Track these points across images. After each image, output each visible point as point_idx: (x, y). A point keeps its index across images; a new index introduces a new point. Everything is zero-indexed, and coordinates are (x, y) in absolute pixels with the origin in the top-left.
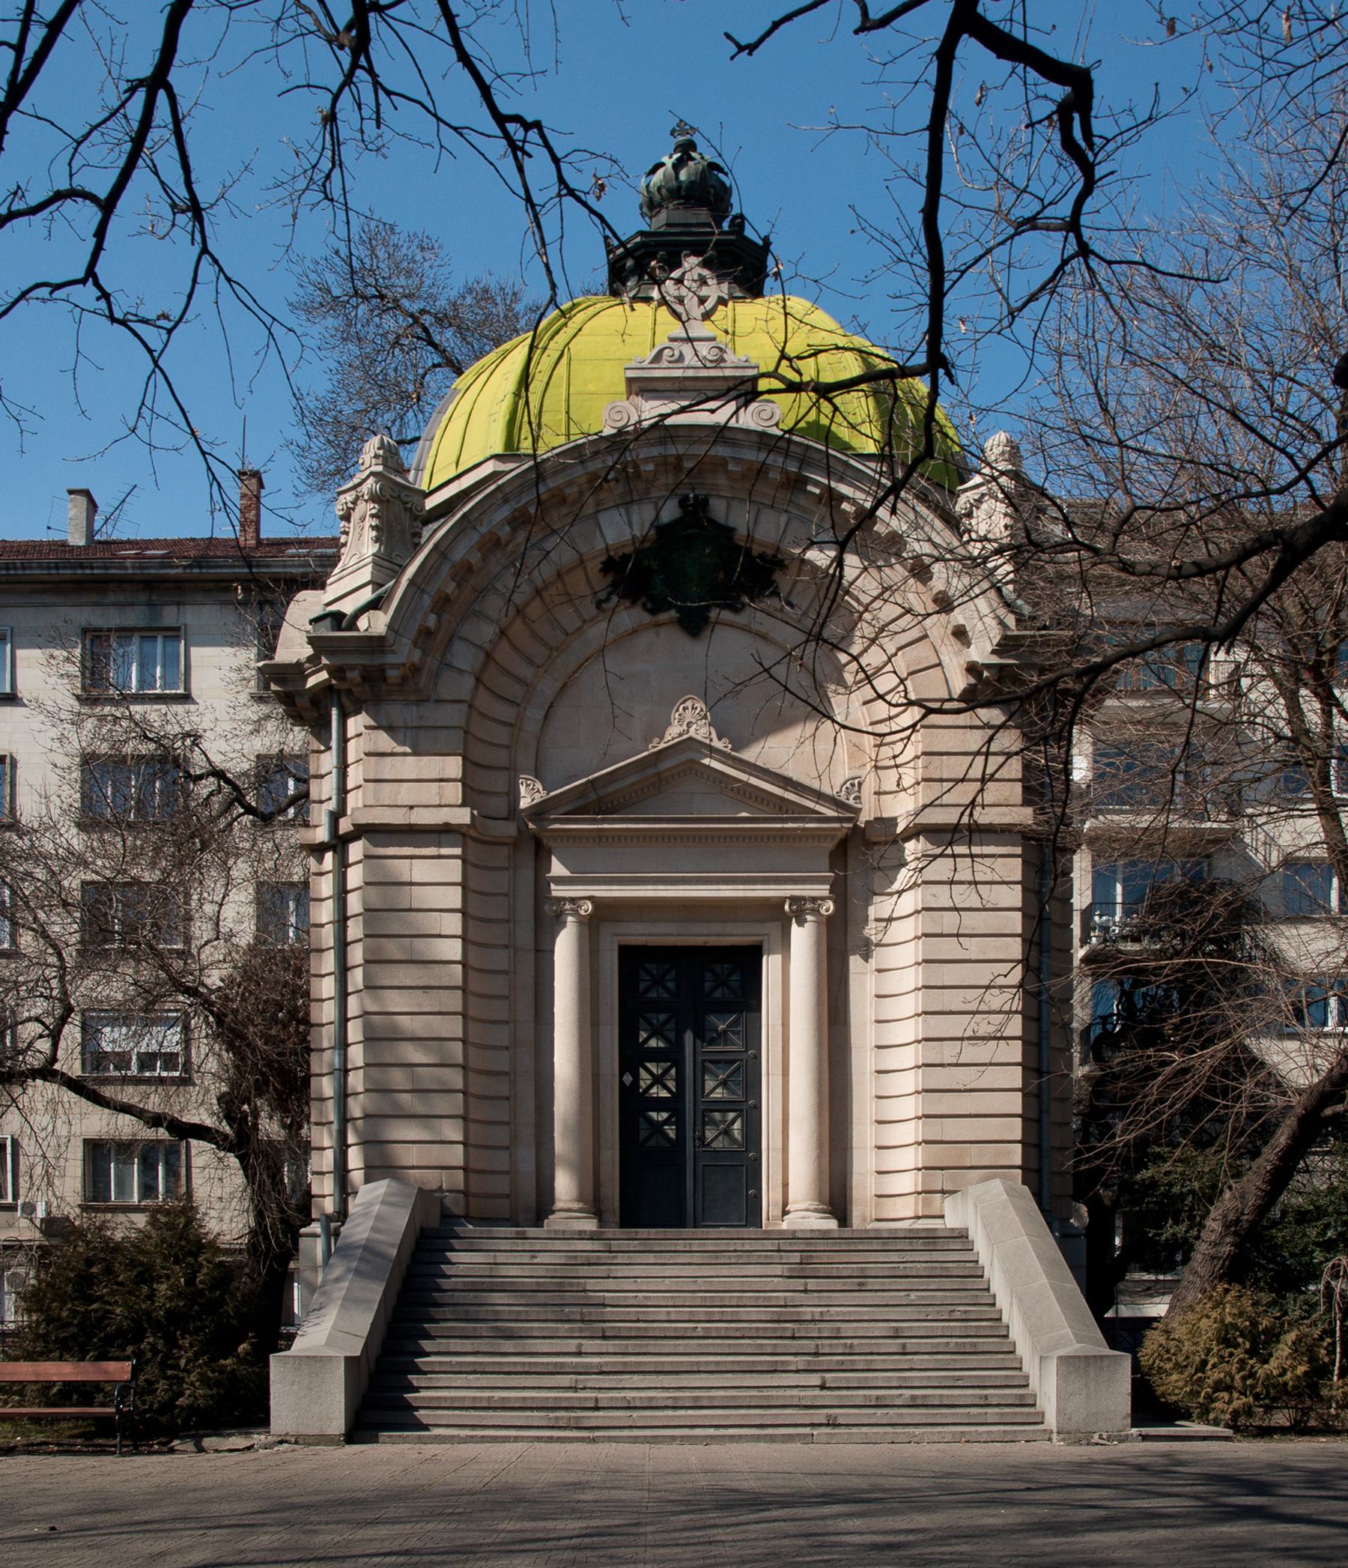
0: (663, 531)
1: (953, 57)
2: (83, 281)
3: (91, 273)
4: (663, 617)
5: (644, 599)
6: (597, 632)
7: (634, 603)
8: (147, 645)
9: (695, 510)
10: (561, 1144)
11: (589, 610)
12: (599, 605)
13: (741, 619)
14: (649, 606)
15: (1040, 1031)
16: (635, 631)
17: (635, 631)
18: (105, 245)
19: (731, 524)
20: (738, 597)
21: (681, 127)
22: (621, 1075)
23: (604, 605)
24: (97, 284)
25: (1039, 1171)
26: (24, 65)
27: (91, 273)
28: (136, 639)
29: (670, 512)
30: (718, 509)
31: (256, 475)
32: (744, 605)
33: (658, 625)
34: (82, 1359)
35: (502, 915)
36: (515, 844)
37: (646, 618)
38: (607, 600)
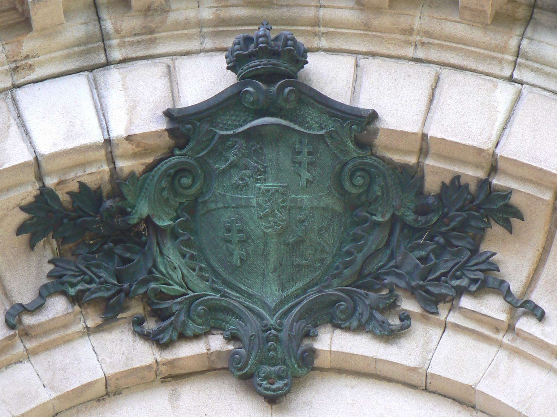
0: (183, 124)
4: (187, 351)
5: (137, 309)
9: (269, 68)
13: (401, 354)
14: (151, 325)
19: (364, 103)
20: (392, 306)
23: (28, 320)
29: (205, 79)
30: (329, 74)
32: (405, 317)
33: (174, 377)
37: (144, 354)
38: (37, 307)
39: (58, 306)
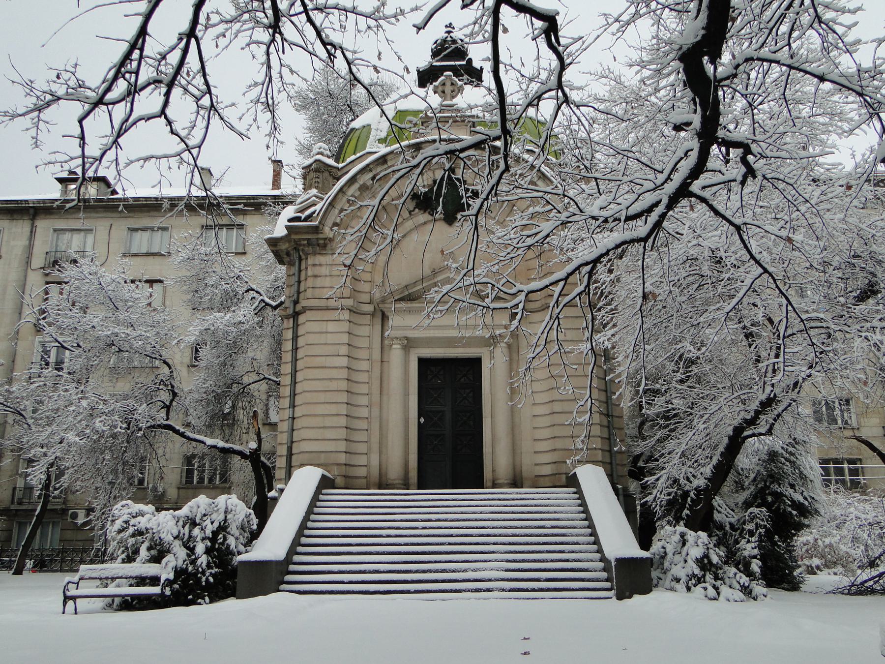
1: (499, 12)
2: (160, 116)
3: (163, 112)
6: (409, 224)
7: (425, 212)
8: (230, 232)
10: (264, 477)
11: (406, 214)
12: (410, 212)
15: (607, 397)
16: (425, 223)
17: (425, 223)
18: (171, 100)
21: (462, 9)
22: (419, 418)
24: (166, 118)
25: (611, 463)
26: (141, 41)
27: (163, 112)
28: (225, 229)
31: (280, 161)
34: (19, 572)
35: (366, 345)
36: (373, 315)
39: (417, 210)
